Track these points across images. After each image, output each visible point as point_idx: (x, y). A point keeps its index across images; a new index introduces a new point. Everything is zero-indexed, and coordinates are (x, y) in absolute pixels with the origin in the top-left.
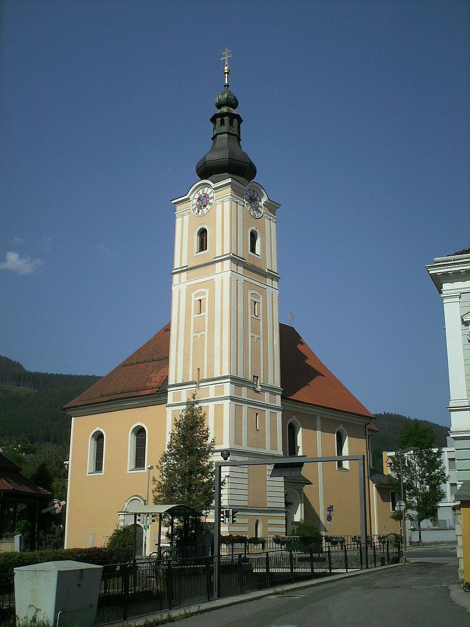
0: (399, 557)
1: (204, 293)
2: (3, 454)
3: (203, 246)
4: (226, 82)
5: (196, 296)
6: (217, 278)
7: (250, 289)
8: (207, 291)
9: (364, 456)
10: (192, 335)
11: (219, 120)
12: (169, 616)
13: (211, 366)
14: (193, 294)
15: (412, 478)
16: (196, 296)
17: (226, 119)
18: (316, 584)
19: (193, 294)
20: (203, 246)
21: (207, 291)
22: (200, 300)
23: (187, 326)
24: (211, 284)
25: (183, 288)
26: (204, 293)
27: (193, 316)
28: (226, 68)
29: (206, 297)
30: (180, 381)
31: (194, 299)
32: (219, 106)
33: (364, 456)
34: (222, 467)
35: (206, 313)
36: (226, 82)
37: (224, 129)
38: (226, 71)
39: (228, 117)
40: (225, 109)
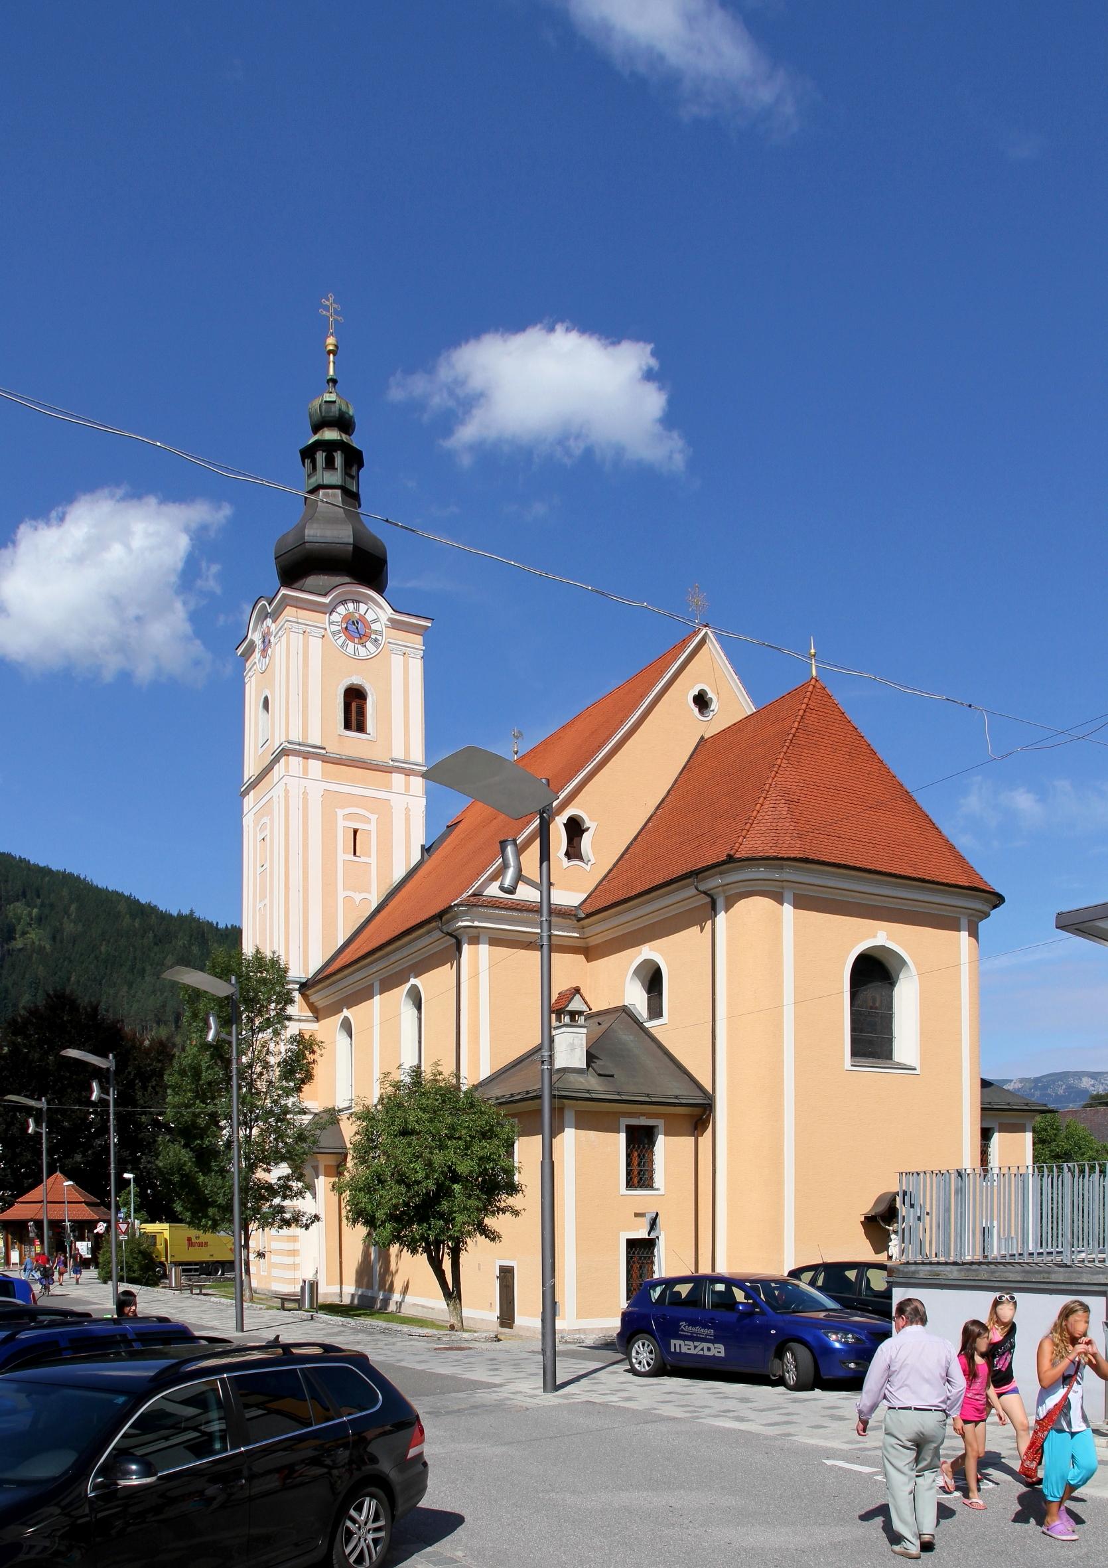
4: (331, 372)
5: (347, 817)
6: (398, 803)
7: (342, 807)
8: (374, 817)
9: (184, 1271)
10: (341, 894)
11: (320, 457)
12: (982, 1355)
14: (340, 813)
16: (347, 817)
17: (339, 458)
19: (340, 813)
21: (374, 817)
22: (355, 832)
24: (383, 808)
26: (368, 821)
28: (331, 340)
29: (370, 828)
31: (343, 827)
32: (316, 428)
33: (184, 1271)
36: (331, 372)
37: (334, 478)
38: (331, 348)
39: (336, 450)
40: (330, 435)
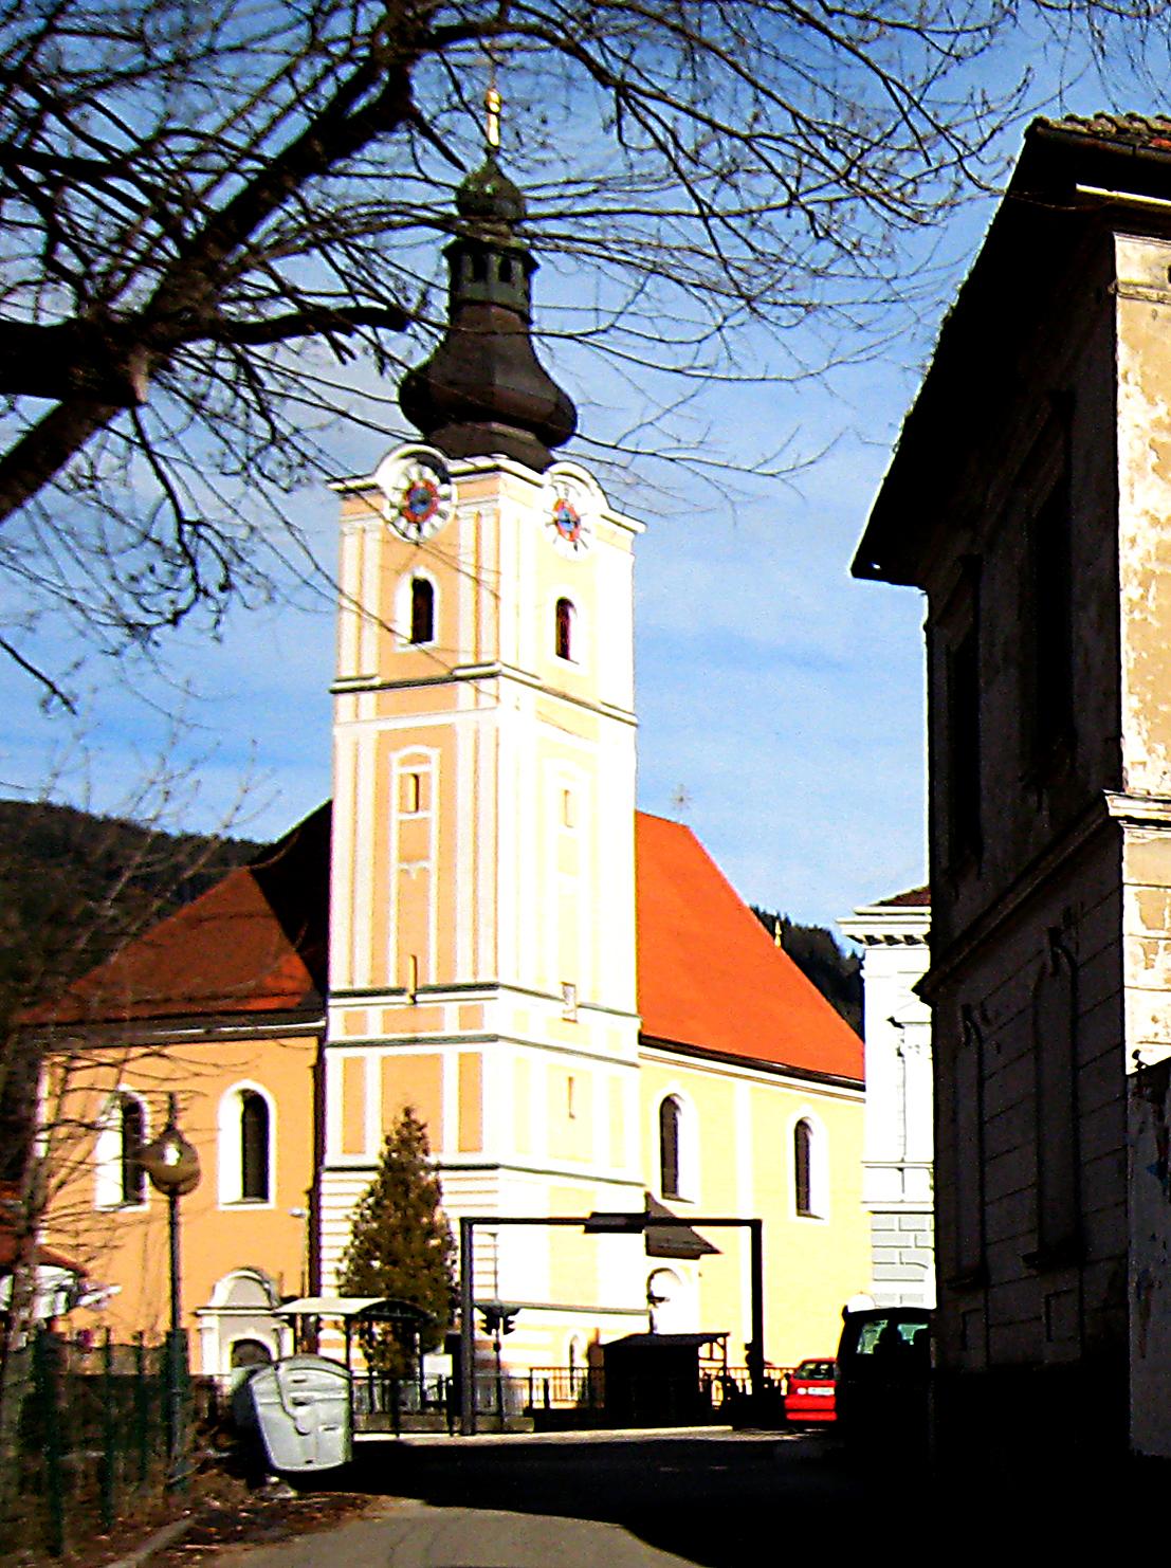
0: (491, 162)
1: (426, 760)
2: (31, 1164)
3: (422, 630)
5: (405, 762)
8: (434, 754)
13: (447, 958)
14: (396, 757)
15: (588, 18)
16: (405, 762)
18: (454, 825)
20: (422, 630)
21: (434, 754)
23: (380, 844)
25: (369, 734)
26: (426, 760)
27: (396, 817)
29: (432, 771)
30: (362, 984)
34: (476, 1228)
35: (432, 813)
